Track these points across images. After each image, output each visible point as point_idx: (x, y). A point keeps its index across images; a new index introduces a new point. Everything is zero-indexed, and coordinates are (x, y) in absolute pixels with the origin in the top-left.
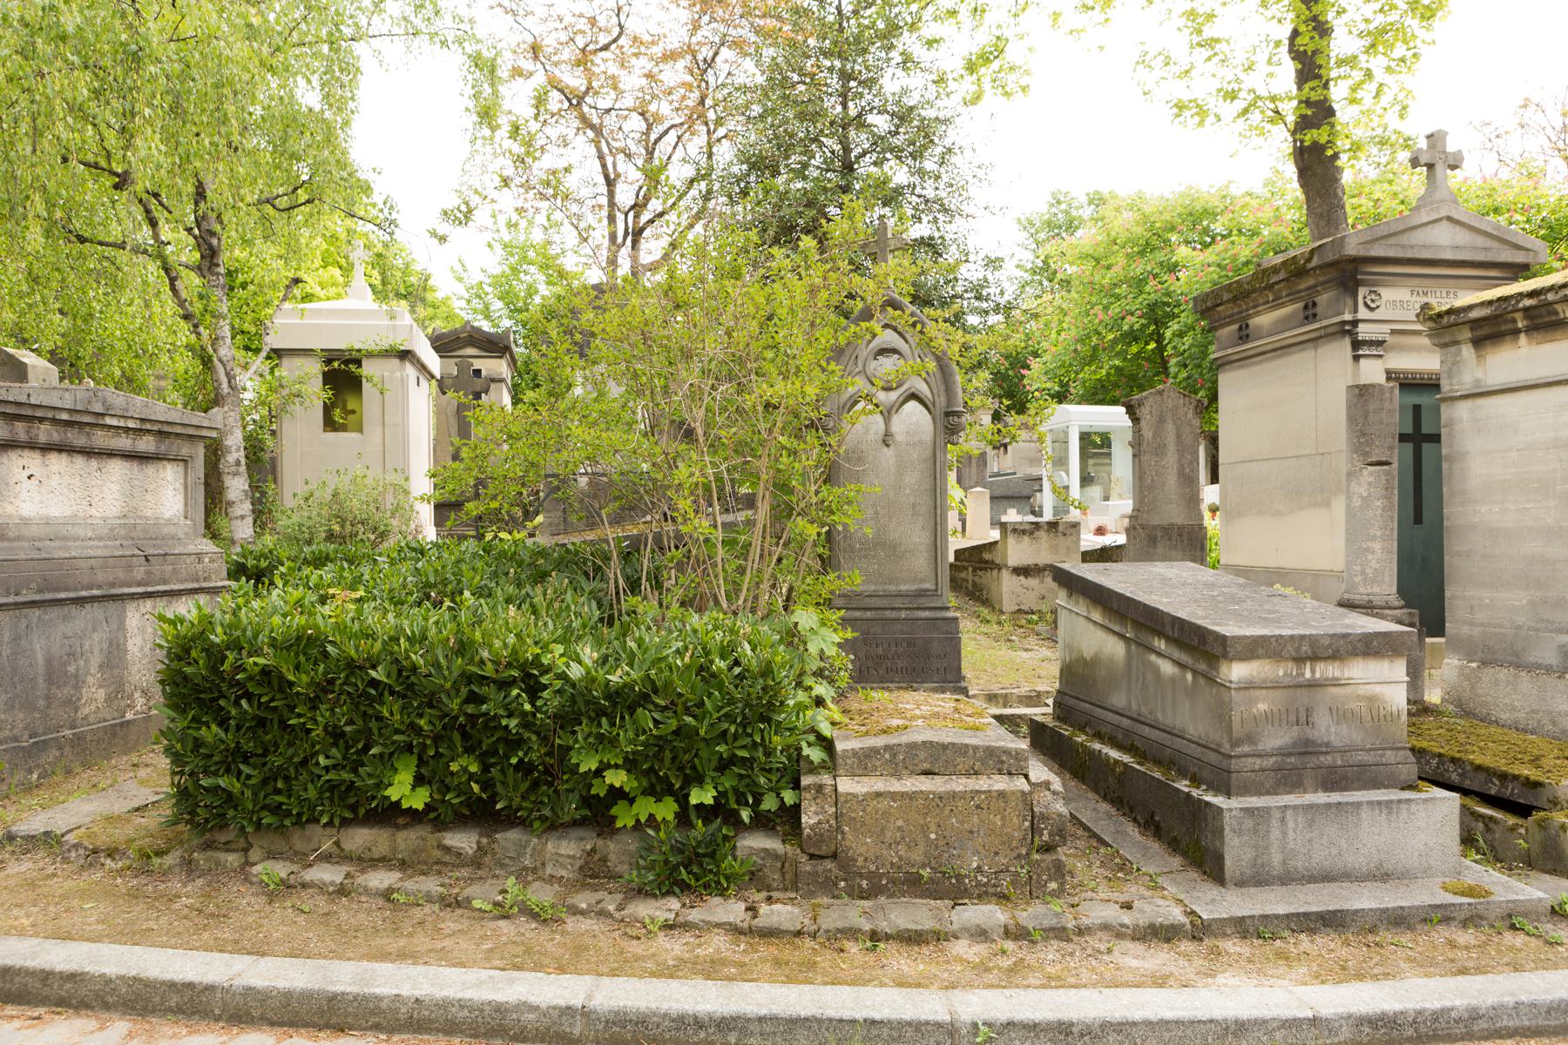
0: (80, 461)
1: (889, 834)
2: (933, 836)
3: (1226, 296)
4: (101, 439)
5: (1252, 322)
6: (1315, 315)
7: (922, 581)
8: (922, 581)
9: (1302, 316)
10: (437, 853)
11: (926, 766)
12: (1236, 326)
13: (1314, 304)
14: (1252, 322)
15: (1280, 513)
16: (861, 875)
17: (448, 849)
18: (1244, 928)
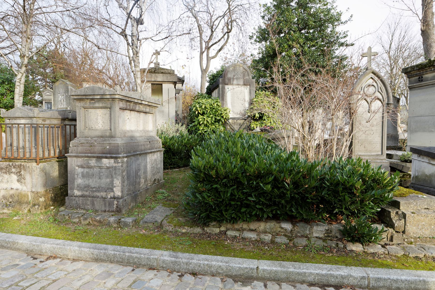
0: (136, 112)
1: (420, 226)
2: (433, 227)
3: (415, 69)
4: (142, 108)
5: (424, 76)
6: (422, 80)
7: (378, 151)
8: (378, 151)
9: (418, 80)
10: (279, 229)
11: (426, 207)
12: (418, 77)
13: (422, 77)
14: (424, 76)
15: (432, 131)
16: (412, 238)
17: (282, 228)
18: (95, 153)
